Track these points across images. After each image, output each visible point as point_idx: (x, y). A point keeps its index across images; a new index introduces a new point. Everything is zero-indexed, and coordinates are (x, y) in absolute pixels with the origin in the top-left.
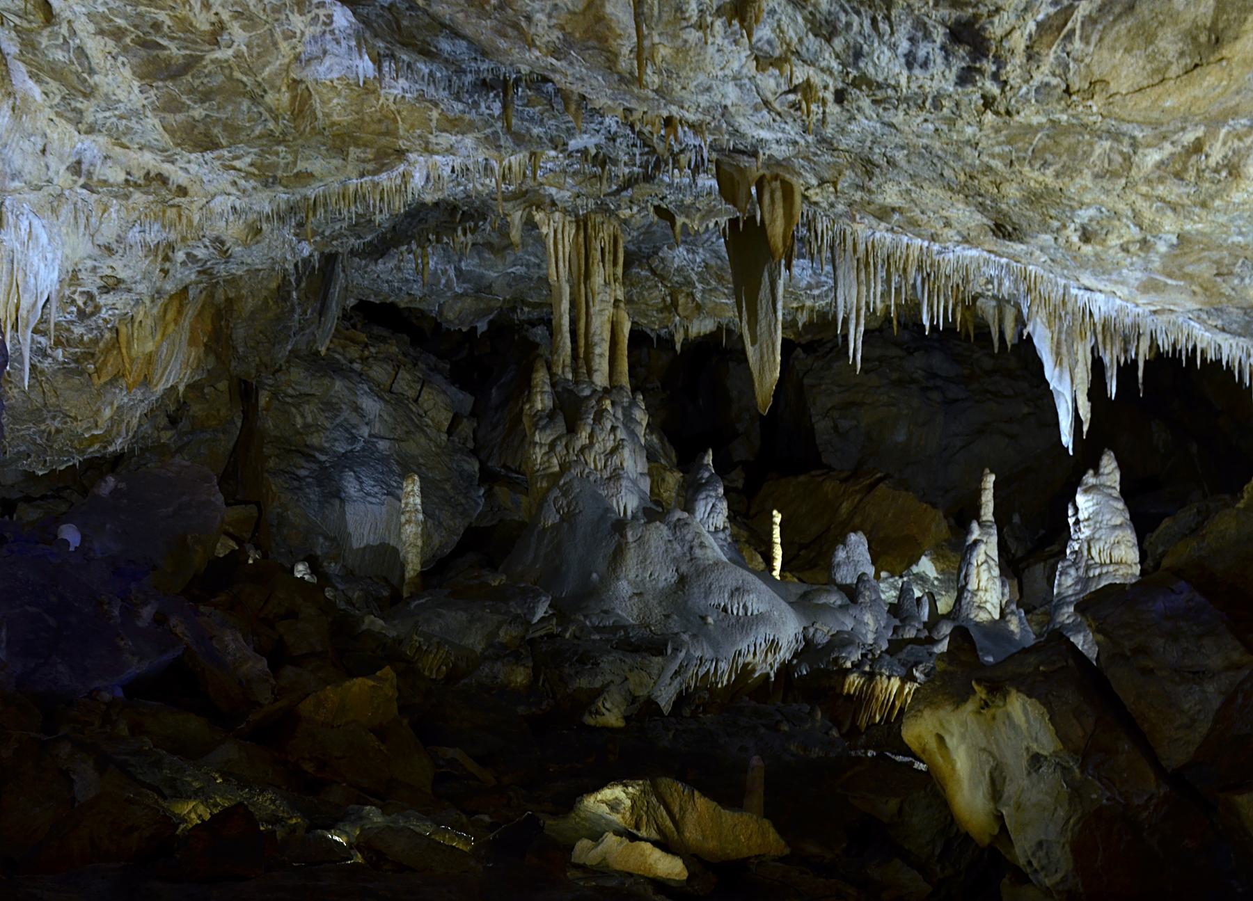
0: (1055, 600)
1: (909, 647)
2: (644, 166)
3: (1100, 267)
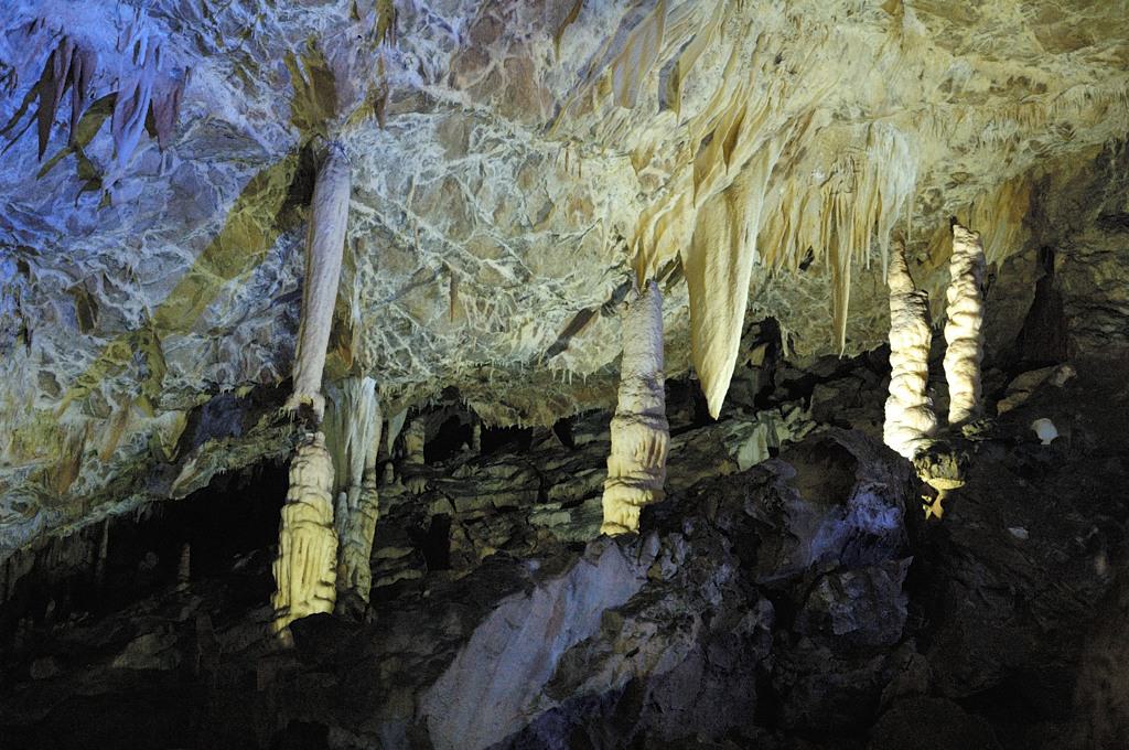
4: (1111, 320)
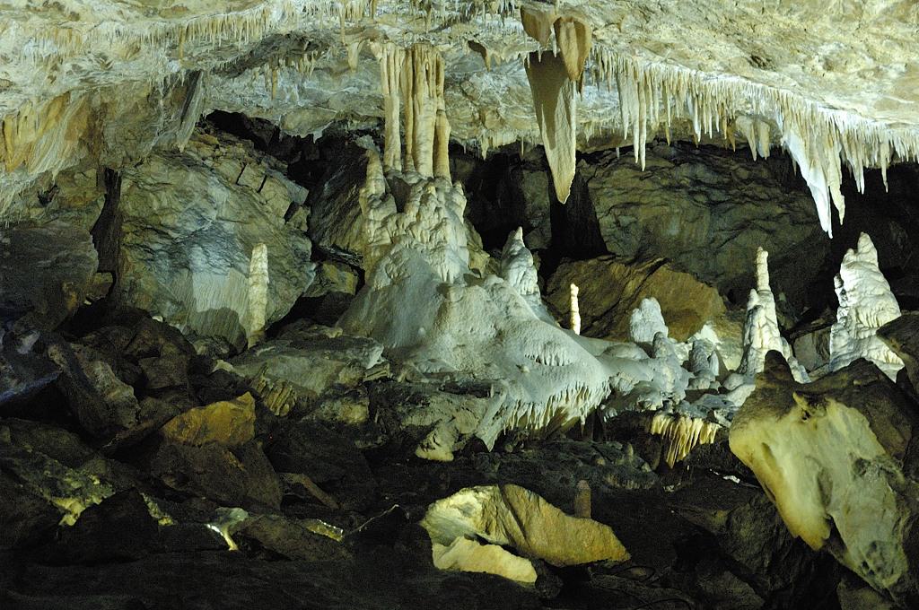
0: (832, 358)
1: (706, 395)
2: (462, 10)
3: (841, 89)
4: (159, 240)
